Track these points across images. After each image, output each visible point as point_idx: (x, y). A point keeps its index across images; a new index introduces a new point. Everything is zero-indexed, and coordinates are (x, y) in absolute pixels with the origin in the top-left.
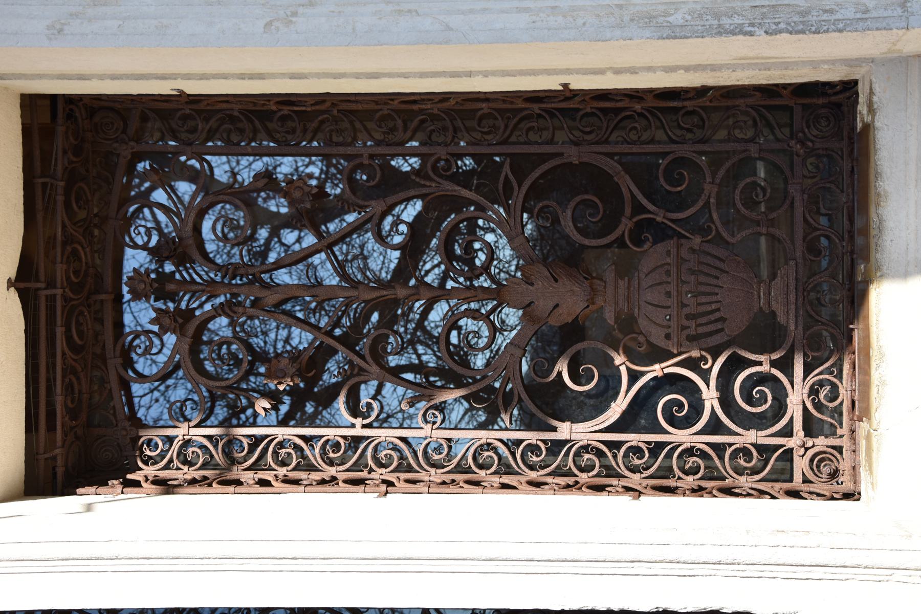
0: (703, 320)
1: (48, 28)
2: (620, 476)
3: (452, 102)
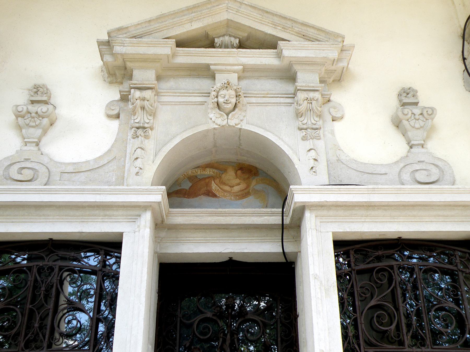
1: (316, 274)
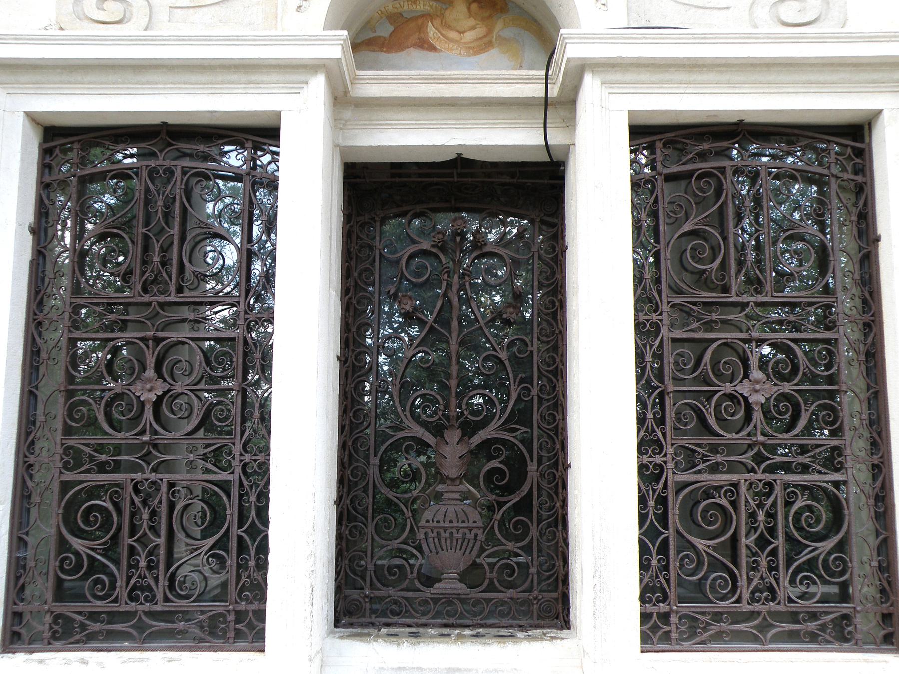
0: (436, 541)
2: (348, 493)
3: (562, 399)
